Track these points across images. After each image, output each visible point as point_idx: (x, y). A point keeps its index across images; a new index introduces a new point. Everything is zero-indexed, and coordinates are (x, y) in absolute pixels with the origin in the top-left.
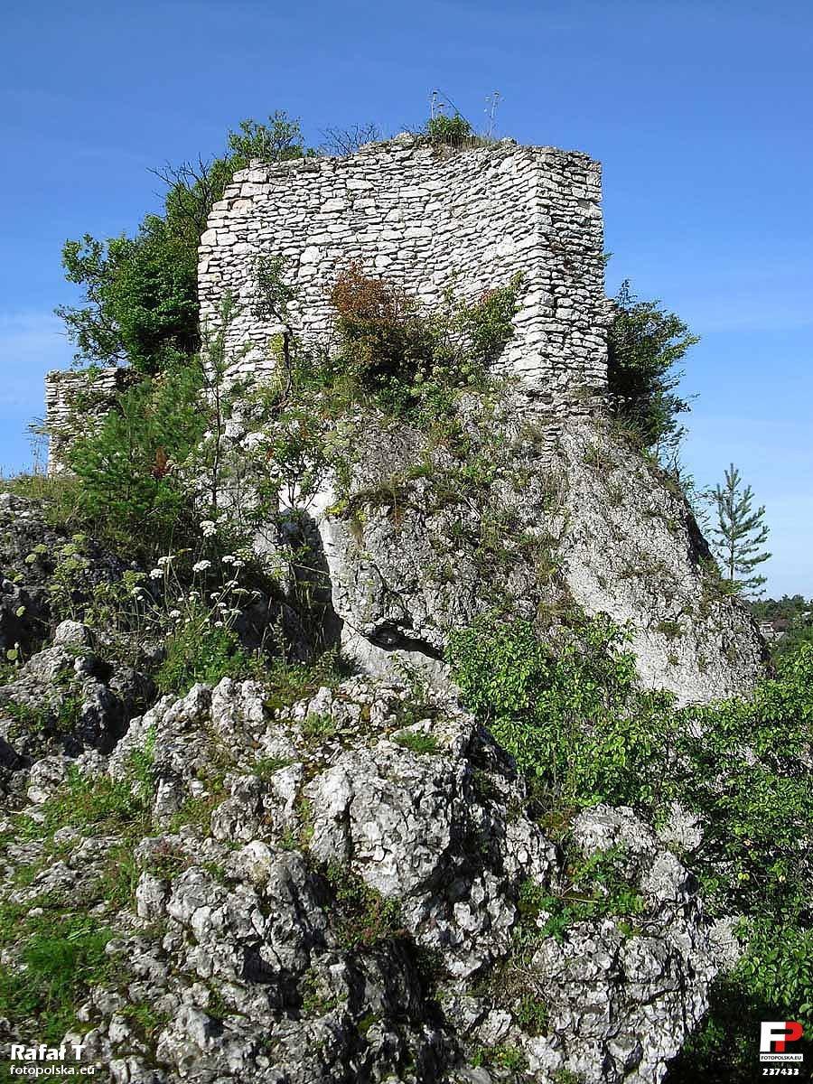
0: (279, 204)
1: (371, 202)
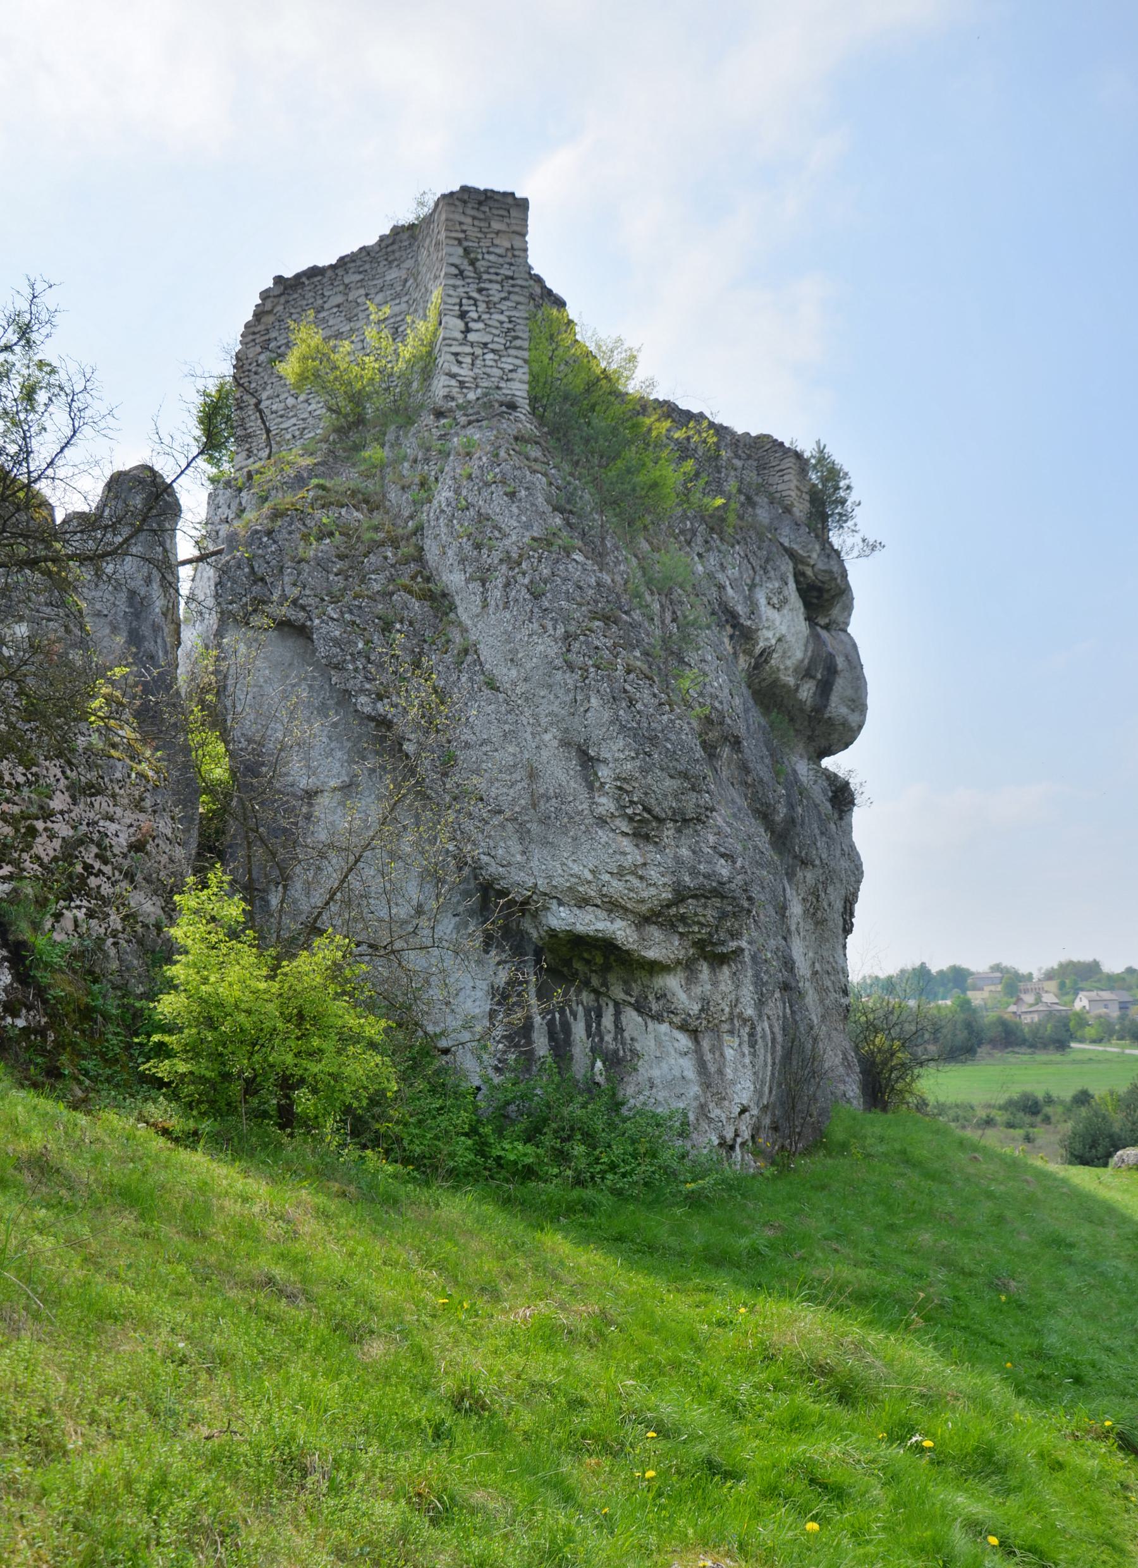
0: (293, 311)
1: (362, 291)
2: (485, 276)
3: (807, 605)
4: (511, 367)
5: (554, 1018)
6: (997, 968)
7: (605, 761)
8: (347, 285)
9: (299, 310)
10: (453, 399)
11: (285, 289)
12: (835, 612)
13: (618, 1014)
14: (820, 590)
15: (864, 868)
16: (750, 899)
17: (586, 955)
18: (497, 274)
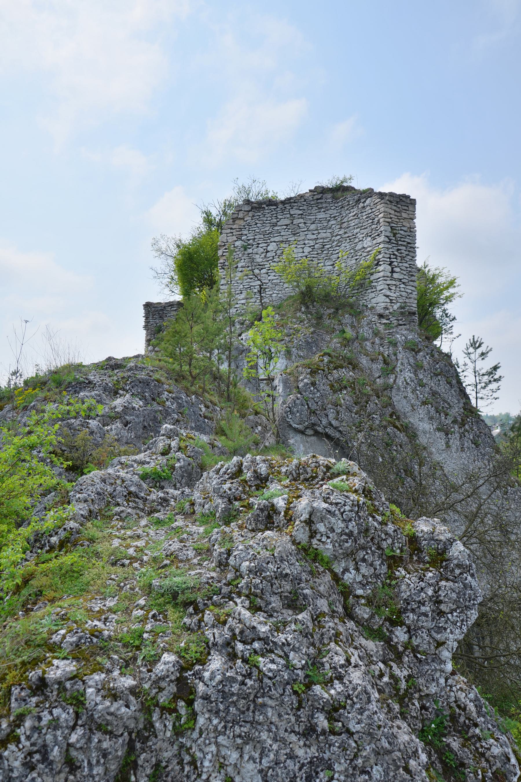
0: (257, 222)
2: (400, 243)
4: (410, 291)
8: (291, 215)
9: (261, 222)
10: (388, 309)
11: (252, 208)
18: (404, 241)
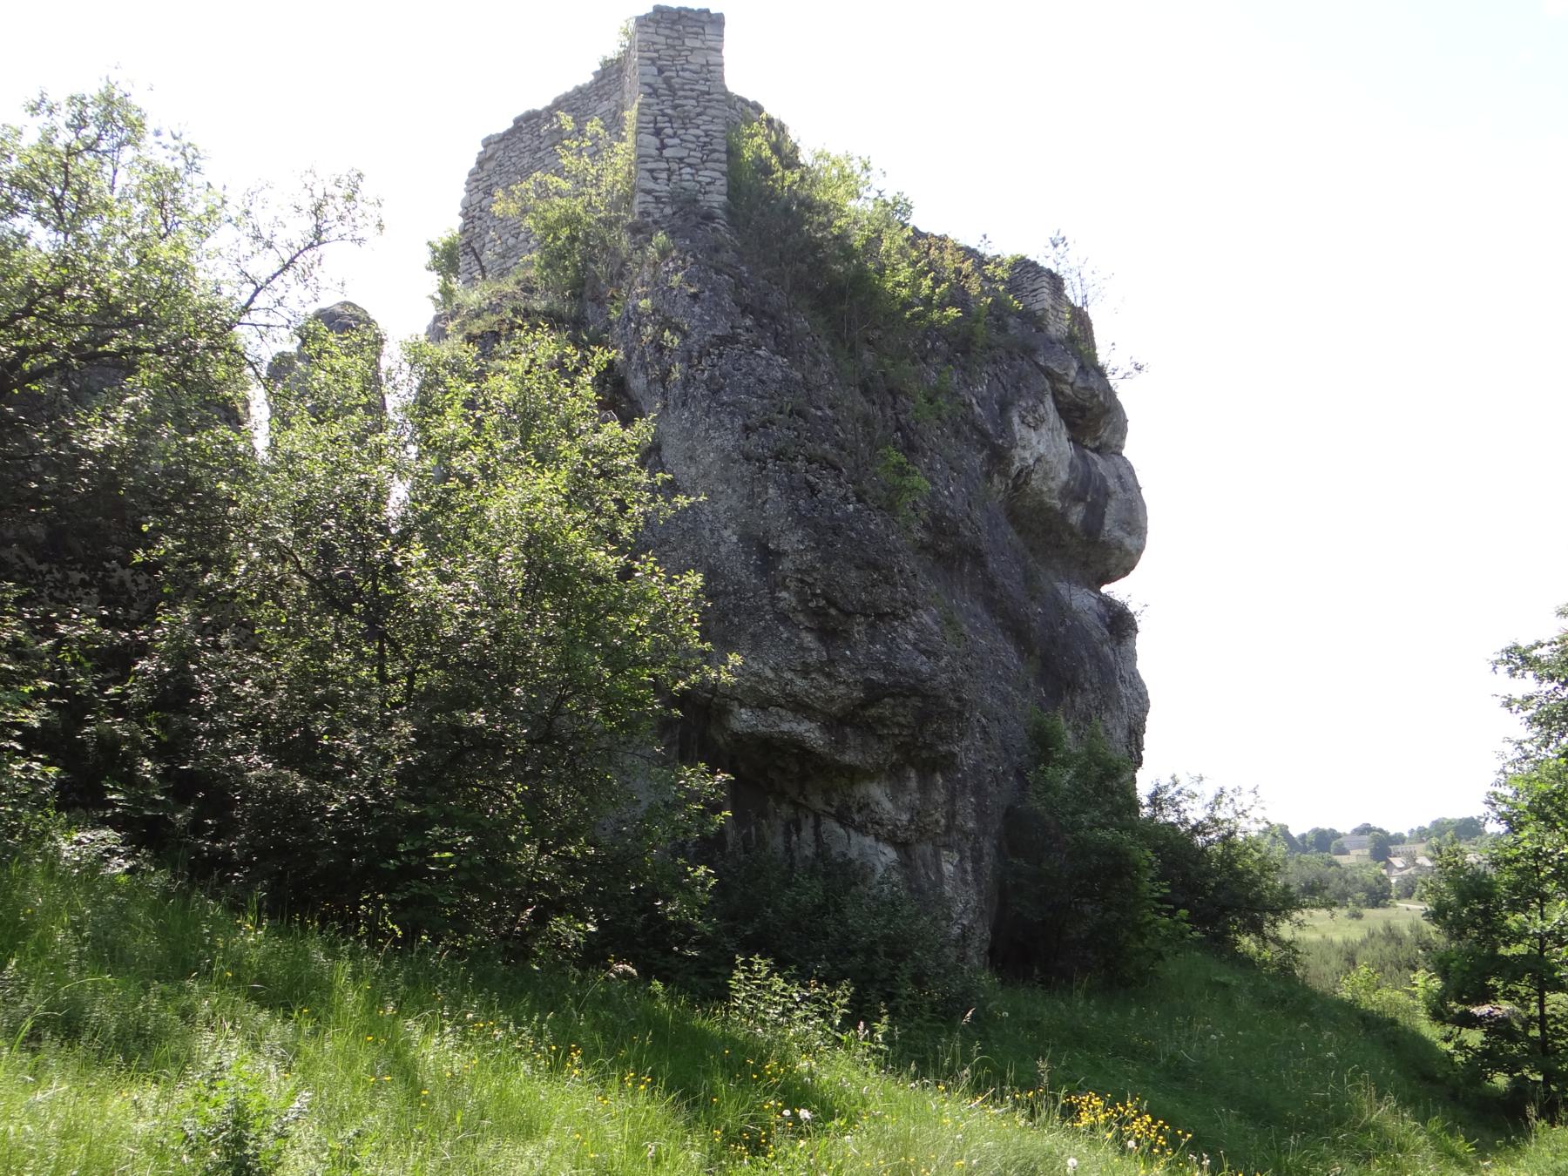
2: (681, 93)
3: (1071, 426)
5: (749, 833)
6: (1366, 830)
7: (785, 553)
12: (1105, 434)
13: (817, 826)
14: (1083, 410)
15: (1150, 696)
16: (959, 699)
17: (779, 763)
